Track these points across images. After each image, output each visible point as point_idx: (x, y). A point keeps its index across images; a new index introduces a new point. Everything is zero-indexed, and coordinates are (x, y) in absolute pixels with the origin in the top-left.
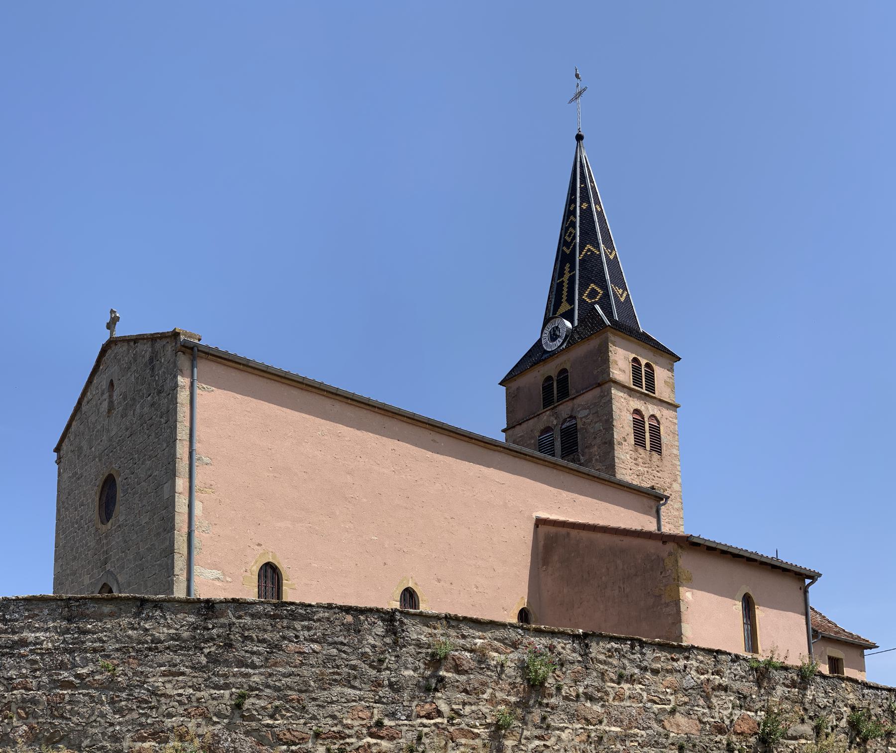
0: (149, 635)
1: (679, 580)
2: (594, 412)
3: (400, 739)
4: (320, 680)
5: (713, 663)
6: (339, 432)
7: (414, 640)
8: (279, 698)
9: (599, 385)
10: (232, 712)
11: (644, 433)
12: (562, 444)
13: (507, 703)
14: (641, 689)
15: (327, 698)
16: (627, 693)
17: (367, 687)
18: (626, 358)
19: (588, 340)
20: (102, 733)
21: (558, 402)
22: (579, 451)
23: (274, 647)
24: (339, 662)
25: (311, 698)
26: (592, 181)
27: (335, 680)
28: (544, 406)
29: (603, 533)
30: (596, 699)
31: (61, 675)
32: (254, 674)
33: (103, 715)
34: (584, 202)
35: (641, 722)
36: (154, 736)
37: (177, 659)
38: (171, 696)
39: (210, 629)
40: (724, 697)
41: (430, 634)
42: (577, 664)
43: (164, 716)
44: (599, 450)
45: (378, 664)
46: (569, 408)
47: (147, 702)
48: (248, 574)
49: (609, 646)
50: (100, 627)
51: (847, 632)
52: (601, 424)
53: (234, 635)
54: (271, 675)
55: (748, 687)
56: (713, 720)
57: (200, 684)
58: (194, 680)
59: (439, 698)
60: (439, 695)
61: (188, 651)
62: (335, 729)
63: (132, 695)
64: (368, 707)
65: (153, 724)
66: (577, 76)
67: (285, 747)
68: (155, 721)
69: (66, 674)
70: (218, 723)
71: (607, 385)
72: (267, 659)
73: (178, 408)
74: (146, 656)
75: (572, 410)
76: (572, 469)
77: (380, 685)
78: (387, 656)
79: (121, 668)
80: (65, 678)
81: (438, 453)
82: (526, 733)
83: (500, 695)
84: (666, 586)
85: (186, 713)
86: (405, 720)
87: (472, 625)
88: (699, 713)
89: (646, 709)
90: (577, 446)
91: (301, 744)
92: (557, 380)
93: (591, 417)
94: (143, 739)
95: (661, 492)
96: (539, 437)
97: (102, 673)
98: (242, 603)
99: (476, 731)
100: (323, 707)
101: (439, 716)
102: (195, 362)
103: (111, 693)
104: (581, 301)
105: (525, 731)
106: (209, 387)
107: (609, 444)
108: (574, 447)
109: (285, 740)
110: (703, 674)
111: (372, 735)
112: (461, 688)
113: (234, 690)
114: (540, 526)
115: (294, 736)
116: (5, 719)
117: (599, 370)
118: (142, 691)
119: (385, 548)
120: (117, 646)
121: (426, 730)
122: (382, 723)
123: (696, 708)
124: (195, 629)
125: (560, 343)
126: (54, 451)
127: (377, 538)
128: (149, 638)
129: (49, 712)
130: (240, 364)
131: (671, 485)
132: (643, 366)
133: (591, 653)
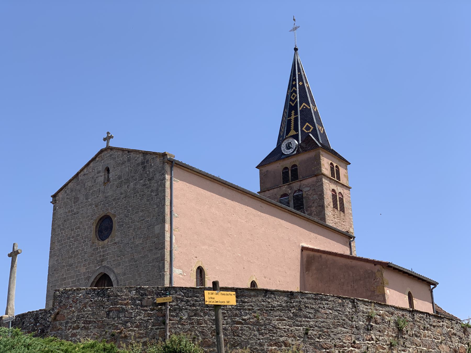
0: (270, 304)
1: (384, 284)
2: (313, 189)
3: (362, 348)
4: (334, 324)
5: (451, 324)
6: (225, 202)
7: (361, 310)
8: (320, 331)
9: (316, 176)
10: (304, 336)
11: (337, 202)
12: (294, 203)
13: (392, 336)
14: (431, 333)
15: (337, 331)
16: (427, 334)
17: (349, 328)
18: (328, 163)
19: (309, 152)
20: (255, 343)
21: (292, 181)
22: (304, 208)
23: (317, 311)
24: (339, 318)
25: (331, 331)
26: (303, 72)
27: (339, 325)
28: (283, 182)
29: (366, 262)
30: (418, 336)
31: (236, 319)
32: (311, 321)
33: (255, 335)
34: (300, 81)
35: (432, 346)
36: (276, 344)
37: (282, 314)
38: (281, 329)
39: (293, 303)
40: (455, 338)
41: (366, 308)
42: (411, 322)
43: (279, 337)
44: (316, 209)
45: (351, 319)
46: (298, 185)
47: (272, 331)
48: (192, 272)
49: (420, 315)
50: (251, 300)
51: (447, 313)
52: (317, 196)
53: (302, 305)
54: (317, 322)
55: (461, 334)
56: (453, 347)
57: (291, 324)
58: (289, 323)
59: (372, 333)
60: (372, 332)
61: (285, 311)
62: (340, 344)
63: (266, 328)
64: (350, 336)
65: (275, 340)
66: (294, 20)
67: (324, 350)
68: (276, 338)
69: (238, 319)
70: (299, 340)
71: (320, 176)
72: (315, 316)
73: (166, 190)
74: (270, 313)
75: (300, 186)
76: (315, 222)
77: (353, 327)
78: (354, 316)
79: (261, 317)
80: (238, 320)
81: (263, 213)
82: (399, 348)
83: (390, 333)
84: (377, 286)
85: (287, 336)
86: (362, 341)
87: (379, 305)
88: (449, 344)
89: (433, 341)
90: (303, 205)
91: (330, 349)
92: (291, 170)
93: (311, 192)
94: (271, 345)
95: (351, 234)
96: (280, 198)
97: (253, 319)
98: (304, 293)
99: (384, 347)
100: (336, 335)
101: (372, 340)
102: (172, 168)
103: (257, 327)
104: (302, 131)
105: (399, 348)
106: (177, 180)
107: (322, 207)
108: (301, 206)
109: (324, 347)
110: (448, 328)
111: (352, 347)
112: (378, 330)
113: (304, 327)
114: (304, 250)
115: (327, 346)
116: (213, 336)
117: (315, 168)
118: (270, 326)
119: (244, 260)
120: (258, 308)
121: (369, 345)
122: (355, 342)
123: (448, 342)
124: (287, 302)
125: (292, 151)
126: (51, 196)
127: (240, 255)
128: (270, 306)
129: (232, 334)
130: (189, 169)
131: (349, 229)
132: (335, 167)
133: (415, 318)
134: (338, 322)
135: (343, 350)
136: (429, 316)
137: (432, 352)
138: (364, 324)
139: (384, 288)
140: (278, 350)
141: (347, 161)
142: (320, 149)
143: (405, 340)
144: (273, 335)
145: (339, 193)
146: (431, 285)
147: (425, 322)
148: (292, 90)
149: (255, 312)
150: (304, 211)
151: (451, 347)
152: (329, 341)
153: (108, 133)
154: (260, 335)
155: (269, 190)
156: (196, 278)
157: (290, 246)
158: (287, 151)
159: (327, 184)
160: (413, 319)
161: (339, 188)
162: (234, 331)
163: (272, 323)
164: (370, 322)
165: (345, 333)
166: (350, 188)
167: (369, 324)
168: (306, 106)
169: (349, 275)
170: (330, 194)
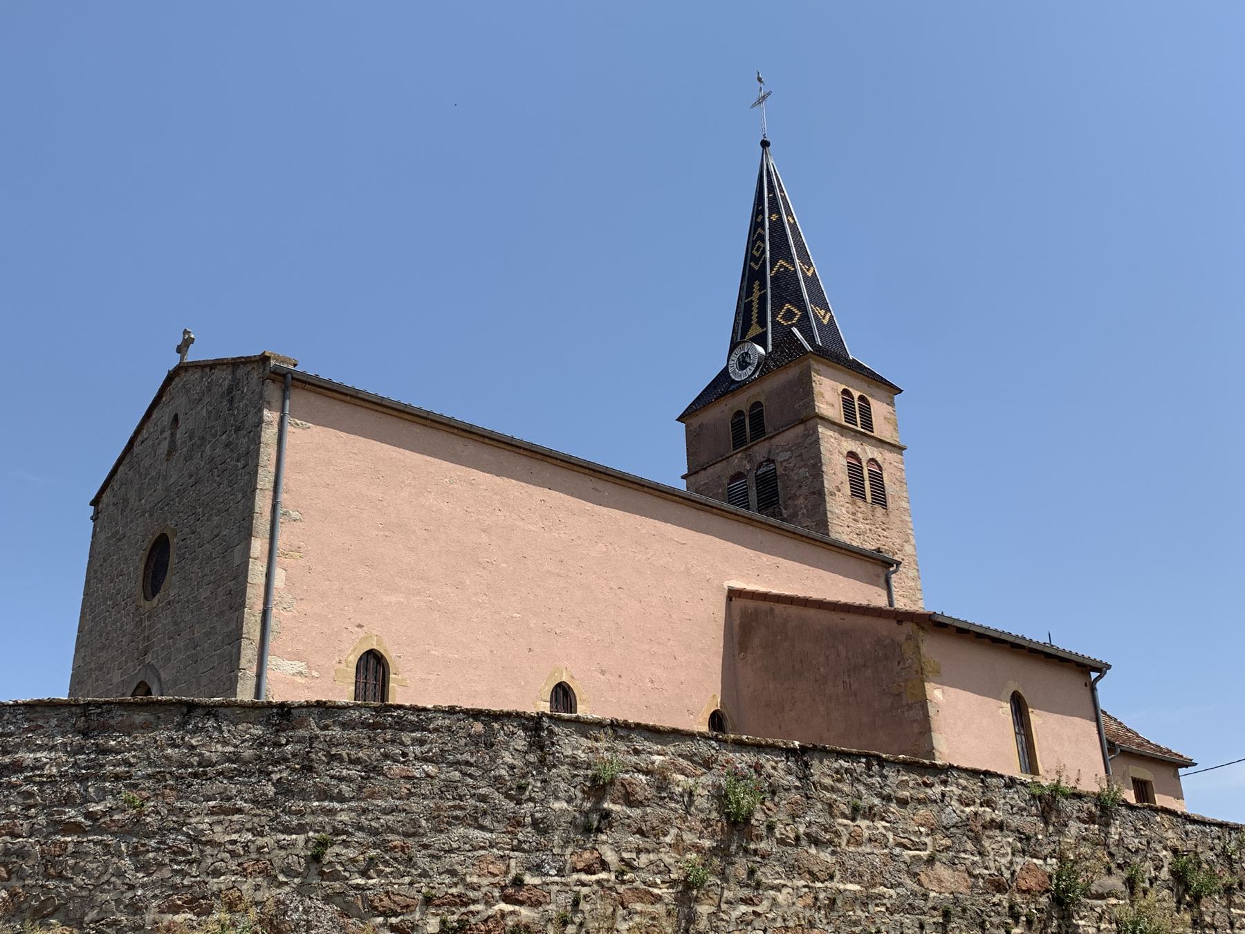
0: (195, 755)
3: (549, 904)
4: (434, 818)
5: (981, 790)
6: (472, 478)
7: (567, 757)
8: (375, 846)
9: (802, 422)
10: (307, 868)
11: (863, 481)
12: (757, 494)
13: (699, 849)
14: (885, 827)
15: (444, 844)
16: (866, 834)
17: (501, 827)
19: (786, 368)
22: (780, 502)
23: (373, 770)
24: (463, 790)
25: (420, 845)
26: (781, 191)
27: (456, 818)
33: (120, 874)
34: (774, 213)
35: (888, 876)
38: (220, 844)
39: (283, 745)
40: (999, 839)
41: (589, 748)
42: (793, 791)
45: (518, 794)
47: (185, 853)
48: (343, 666)
49: (836, 765)
50: (128, 743)
51: (1153, 745)
55: (1030, 823)
56: (987, 872)
57: (263, 826)
58: (256, 820)
59: (604, 843)
60: (604, 837)
61: (249, 777)
64: (502, 857)
65: (191, 887)
66: (760, 80)
67: (381, 919)
68: (195, 882)
69: (73, 813)
70: (286, 884)
72: (360, 788)
74: (190, 785)
75: (770, 452)
77: (519, 824)
78: (531, 780)
79: (152, 804)
80: (70, 818)
81: (600, 505)
82: (728, 894)
83: (689, 838)
84: (906, 680)
86: (556, 875)
87: (647, 734)
88: (967, 862)
89: (893, 857)
90: (777, 496)
91: (403, 914)
93: (793, 460)
94: (176, 910)
96: (729, 485)
98: (330, 707)
99: (656, 891)
100: (438, 858)
101: (604, 870)
102: (287, 393)
103: (135, 840)
104: (775, 323)
106: (304, 423)
107: (819, 495)
109: (381, 909)
110: (968, 805)
111: (507, 899)
113: (311, 834)
114: (733, 599)
115: (395, 902)
118: (180, 837)
119: (531, 629)
120: (150, 771)
121: (585, 890)
122: (522, 881)
123: (963, 855)
124: (262, 744)
126: (91, 504)
129: (42, 869)
130: (347, 395)
131: (902, 547)
132: (856, 400)
134: (455, 807)
135: (463, 914)
136: (882, 767)
137: (887, 896)
138: (571, 808)
139: (924, 685)
140: (195, 928)
141: (891, 385)
142: (810, 357)
143: (759, 860)
144: (186, 868)
145: (869, 461)
146: (1092, 673)
147: (862, 788)
148: (755, 236)
149: (135, 786)
150: (780, 508)
151: (977, 872)
152: (404, 884)
153: (186, 332)
154: (137, 870)
155: (705, 469)
156: (356, 681)
157: (691, 589)
158: (740, 372)
159: (832, 440)
160: (804, 778)
161: (868, 448)
162: (48, 857)
163: (190, 824)
164: (600, 799)
165: (483, 848)
166: (903, 449)
167: (596, 808)
168: (785, 267)
169: (838, 656)
170: (842, 463)
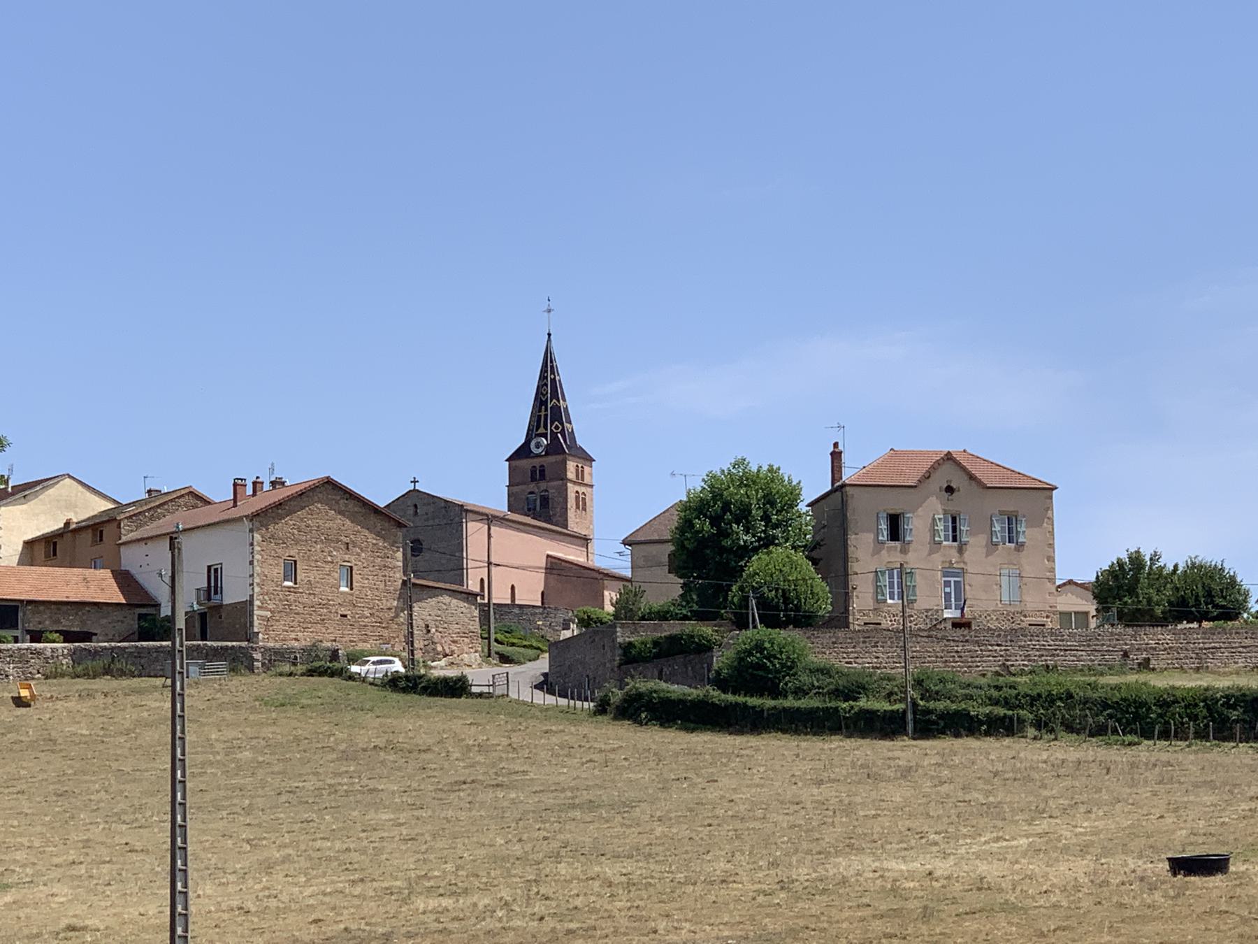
9: (562, 479)
104: (551, 430)
